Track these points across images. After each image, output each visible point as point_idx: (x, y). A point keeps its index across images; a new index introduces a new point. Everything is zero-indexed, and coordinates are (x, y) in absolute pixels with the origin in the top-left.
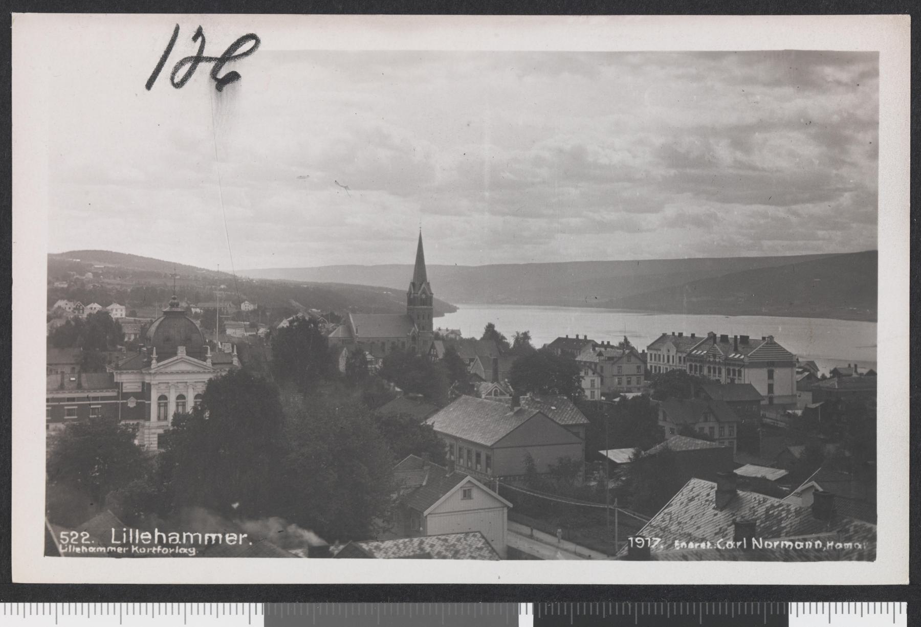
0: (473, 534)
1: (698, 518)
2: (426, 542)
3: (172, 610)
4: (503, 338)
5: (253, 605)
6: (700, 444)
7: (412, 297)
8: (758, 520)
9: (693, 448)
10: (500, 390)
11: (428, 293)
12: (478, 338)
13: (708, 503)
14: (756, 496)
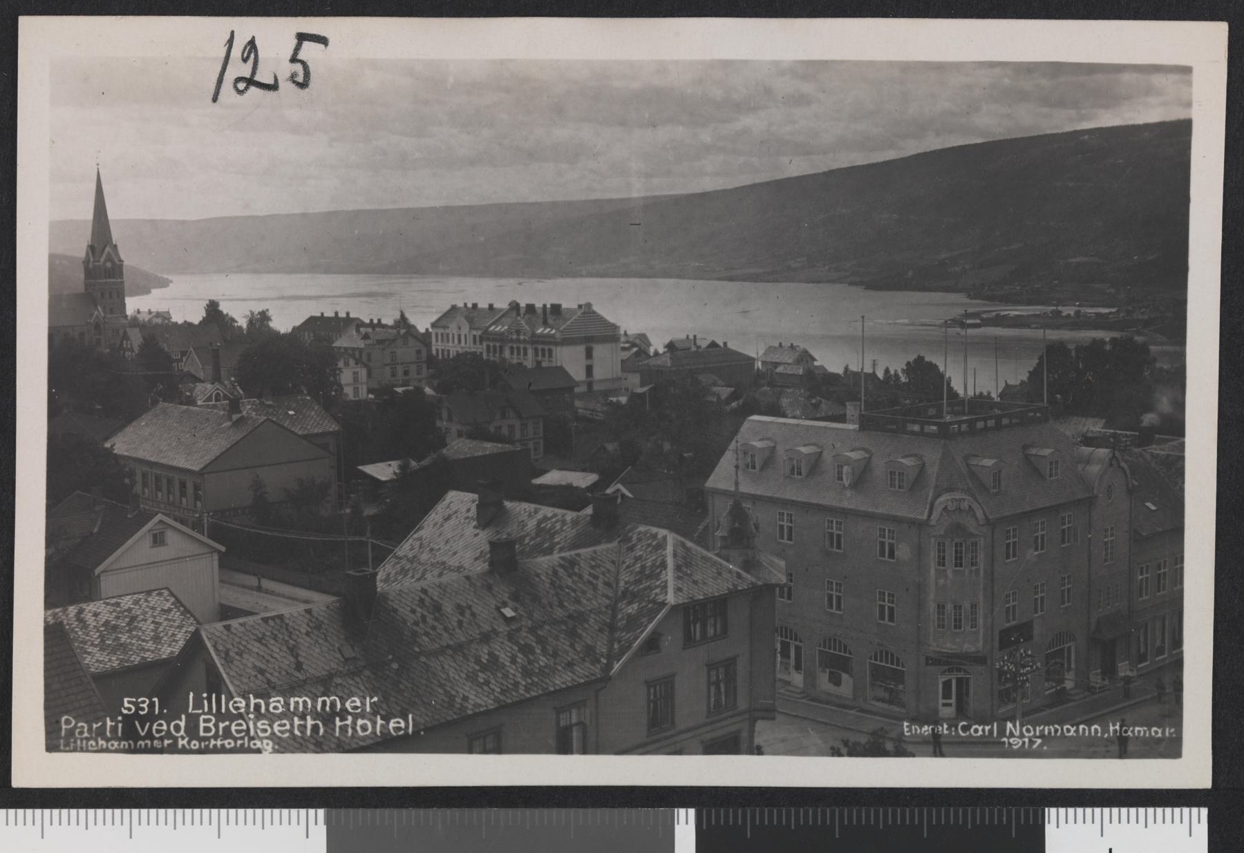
0: (157, 592)
1: (455, 541)
2: (87, 611)
4: (233, 320)
6: (489, 447)
7: (91, 266)
8: (528, 536)
9: (480, 454)
10: (223, 393)
11: (116, 260)
12: (196, 322)
13: (467, 521)
14: (527, 507)
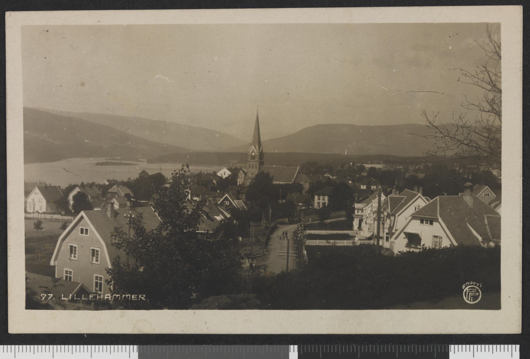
3: (84, 349)
5: (131, 346)
